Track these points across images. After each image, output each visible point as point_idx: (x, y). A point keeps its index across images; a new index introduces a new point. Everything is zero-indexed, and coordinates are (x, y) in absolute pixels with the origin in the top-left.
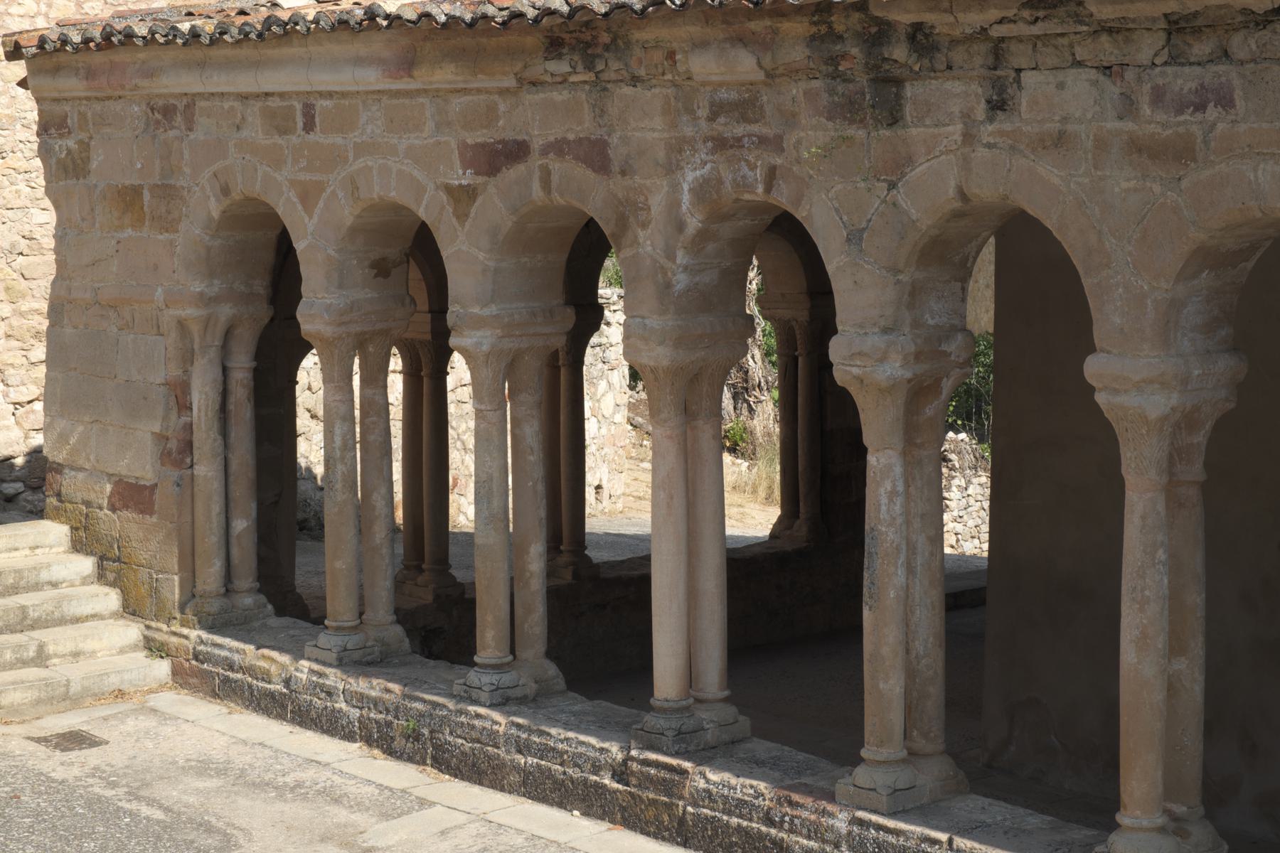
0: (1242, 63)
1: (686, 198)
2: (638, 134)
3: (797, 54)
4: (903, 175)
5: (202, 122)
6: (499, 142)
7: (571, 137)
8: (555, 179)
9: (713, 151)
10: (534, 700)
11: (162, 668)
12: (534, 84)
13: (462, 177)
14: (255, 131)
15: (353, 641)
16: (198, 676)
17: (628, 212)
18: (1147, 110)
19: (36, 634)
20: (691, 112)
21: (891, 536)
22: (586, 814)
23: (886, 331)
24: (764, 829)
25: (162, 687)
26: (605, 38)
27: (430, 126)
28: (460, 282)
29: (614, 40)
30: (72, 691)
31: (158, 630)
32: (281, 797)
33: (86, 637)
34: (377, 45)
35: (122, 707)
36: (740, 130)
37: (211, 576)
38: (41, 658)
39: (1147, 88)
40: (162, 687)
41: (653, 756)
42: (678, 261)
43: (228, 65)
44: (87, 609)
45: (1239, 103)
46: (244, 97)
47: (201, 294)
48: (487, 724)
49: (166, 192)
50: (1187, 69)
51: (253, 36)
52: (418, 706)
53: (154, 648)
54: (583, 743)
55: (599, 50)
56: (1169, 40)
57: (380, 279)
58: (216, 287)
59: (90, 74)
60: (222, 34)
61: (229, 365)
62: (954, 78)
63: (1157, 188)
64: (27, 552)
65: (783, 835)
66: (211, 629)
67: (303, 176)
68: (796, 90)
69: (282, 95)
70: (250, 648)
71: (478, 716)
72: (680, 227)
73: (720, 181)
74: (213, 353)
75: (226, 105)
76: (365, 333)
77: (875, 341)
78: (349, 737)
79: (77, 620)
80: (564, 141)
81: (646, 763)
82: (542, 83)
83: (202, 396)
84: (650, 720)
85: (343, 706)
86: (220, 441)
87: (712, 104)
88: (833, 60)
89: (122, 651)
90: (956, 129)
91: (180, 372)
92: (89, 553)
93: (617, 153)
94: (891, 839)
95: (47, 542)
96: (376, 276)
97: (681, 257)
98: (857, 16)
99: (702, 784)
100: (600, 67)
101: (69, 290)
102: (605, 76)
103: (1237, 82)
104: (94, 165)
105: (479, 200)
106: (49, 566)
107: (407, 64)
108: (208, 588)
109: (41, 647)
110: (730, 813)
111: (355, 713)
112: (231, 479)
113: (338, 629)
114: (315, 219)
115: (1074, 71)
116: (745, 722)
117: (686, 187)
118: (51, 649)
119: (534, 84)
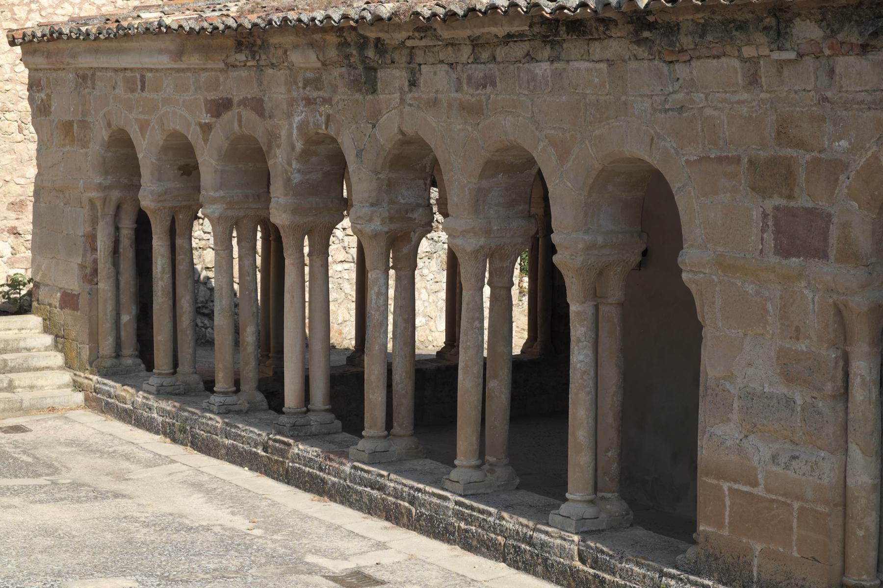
0: (499, 63)
1: (295, 131)
2: (275, 96)
3: (332, 53)
4: (378, 120)
5: (99, 84)
6: (221, 99)
7: (249, 96)
8: (243, 120)
9: (305, 106)
10: (247, 412)
11: (80, 397)
12: (233, 66)
13: (206, 119)
14: (120, 91)
15: (167, 381)
16: (100, 404)
17: (273, 136)
18: (465, 88)
19: (12, 376)
20: (296, 84)
21: (377, 317)
22: (250, 469)
23: (372, 205)
24: (318, 473)
25: (78, 407)
26: (259, 42)
27: (192, 88)
28: (208, 176)
29: (263, 43)
30: (24, 406)
31: (80, 376)
32: (101, 457)
33: (38, 378)
34: (167, 43)
35: (51, 415)
36: (315, 94)
37: (107, 345)
38: (11, 388)
39: (465, 76)
40: (78, 407)
41: (278, 437)
42: (294, 167)
43: (109, 52)
44: (44, 364)
45: (498, 84)
46: (116, 70)
47: (100, 184)
48: (214, 423)
49: (84, 124)
50: (479, 66)
51: (112, 36)
52: (186, 414)
53: (77, 386)
54: (251, 431)
55: (256, 49)
56: (473, 50)
57: (185, 176)
58: (109, 180)
59: (49, 55)
60: (100, 34)
61: (120, 226)
62: (396, 68)
63: (470, 129)
64: (17, 331)
65: (325, 476)
66: (105, 375)
67: (142, 117)
68: (336, 72)
69: (132, 70)
70: (118, 385)
71: (211, 419)
72: (293, 147)
73: (308, 123)
74: (109, 219)
75: (109, 75)
76: (175, 207)
77: (367, 210)
78: (157, 433)
79: (37, 369)
80: (246, 99)
81: (275, 441)
82: (237, 66)
83: (103, 243)
84: (283, 419)
85: (155, 415)
86: (112, 269)
87: (304, 80)
88: (348, 57)
89: (59, 387)
90: (397, 95)
91: (90, 229)
92: (51, 334)
93: (268, 106)
94: (366, 475)
95: (28, 326)
96: (182, 174)
97: (295, 164)
98: (354, 33)
99: (296, 451)
100: (257, 58)
101: (42, 181)
102: (261, 63)
103: (497, 73)
104: (53, 108)
105: (213, 131)
106: (25, 339)
107: (179, 54)
108: (105, 353)
109: (11, 382)
110: (306, 466)
111: (160, 419)
112: (121, 291)
113: (159, 374)
114: (146, 142)
115: (439, 65)
116: (338, 424)
117: (295, 126)
118: (17, 383)
119: (233, 66)
